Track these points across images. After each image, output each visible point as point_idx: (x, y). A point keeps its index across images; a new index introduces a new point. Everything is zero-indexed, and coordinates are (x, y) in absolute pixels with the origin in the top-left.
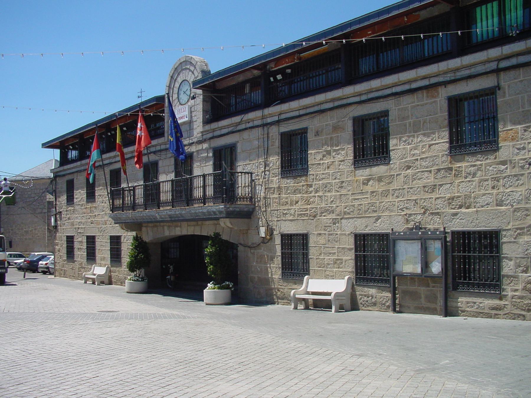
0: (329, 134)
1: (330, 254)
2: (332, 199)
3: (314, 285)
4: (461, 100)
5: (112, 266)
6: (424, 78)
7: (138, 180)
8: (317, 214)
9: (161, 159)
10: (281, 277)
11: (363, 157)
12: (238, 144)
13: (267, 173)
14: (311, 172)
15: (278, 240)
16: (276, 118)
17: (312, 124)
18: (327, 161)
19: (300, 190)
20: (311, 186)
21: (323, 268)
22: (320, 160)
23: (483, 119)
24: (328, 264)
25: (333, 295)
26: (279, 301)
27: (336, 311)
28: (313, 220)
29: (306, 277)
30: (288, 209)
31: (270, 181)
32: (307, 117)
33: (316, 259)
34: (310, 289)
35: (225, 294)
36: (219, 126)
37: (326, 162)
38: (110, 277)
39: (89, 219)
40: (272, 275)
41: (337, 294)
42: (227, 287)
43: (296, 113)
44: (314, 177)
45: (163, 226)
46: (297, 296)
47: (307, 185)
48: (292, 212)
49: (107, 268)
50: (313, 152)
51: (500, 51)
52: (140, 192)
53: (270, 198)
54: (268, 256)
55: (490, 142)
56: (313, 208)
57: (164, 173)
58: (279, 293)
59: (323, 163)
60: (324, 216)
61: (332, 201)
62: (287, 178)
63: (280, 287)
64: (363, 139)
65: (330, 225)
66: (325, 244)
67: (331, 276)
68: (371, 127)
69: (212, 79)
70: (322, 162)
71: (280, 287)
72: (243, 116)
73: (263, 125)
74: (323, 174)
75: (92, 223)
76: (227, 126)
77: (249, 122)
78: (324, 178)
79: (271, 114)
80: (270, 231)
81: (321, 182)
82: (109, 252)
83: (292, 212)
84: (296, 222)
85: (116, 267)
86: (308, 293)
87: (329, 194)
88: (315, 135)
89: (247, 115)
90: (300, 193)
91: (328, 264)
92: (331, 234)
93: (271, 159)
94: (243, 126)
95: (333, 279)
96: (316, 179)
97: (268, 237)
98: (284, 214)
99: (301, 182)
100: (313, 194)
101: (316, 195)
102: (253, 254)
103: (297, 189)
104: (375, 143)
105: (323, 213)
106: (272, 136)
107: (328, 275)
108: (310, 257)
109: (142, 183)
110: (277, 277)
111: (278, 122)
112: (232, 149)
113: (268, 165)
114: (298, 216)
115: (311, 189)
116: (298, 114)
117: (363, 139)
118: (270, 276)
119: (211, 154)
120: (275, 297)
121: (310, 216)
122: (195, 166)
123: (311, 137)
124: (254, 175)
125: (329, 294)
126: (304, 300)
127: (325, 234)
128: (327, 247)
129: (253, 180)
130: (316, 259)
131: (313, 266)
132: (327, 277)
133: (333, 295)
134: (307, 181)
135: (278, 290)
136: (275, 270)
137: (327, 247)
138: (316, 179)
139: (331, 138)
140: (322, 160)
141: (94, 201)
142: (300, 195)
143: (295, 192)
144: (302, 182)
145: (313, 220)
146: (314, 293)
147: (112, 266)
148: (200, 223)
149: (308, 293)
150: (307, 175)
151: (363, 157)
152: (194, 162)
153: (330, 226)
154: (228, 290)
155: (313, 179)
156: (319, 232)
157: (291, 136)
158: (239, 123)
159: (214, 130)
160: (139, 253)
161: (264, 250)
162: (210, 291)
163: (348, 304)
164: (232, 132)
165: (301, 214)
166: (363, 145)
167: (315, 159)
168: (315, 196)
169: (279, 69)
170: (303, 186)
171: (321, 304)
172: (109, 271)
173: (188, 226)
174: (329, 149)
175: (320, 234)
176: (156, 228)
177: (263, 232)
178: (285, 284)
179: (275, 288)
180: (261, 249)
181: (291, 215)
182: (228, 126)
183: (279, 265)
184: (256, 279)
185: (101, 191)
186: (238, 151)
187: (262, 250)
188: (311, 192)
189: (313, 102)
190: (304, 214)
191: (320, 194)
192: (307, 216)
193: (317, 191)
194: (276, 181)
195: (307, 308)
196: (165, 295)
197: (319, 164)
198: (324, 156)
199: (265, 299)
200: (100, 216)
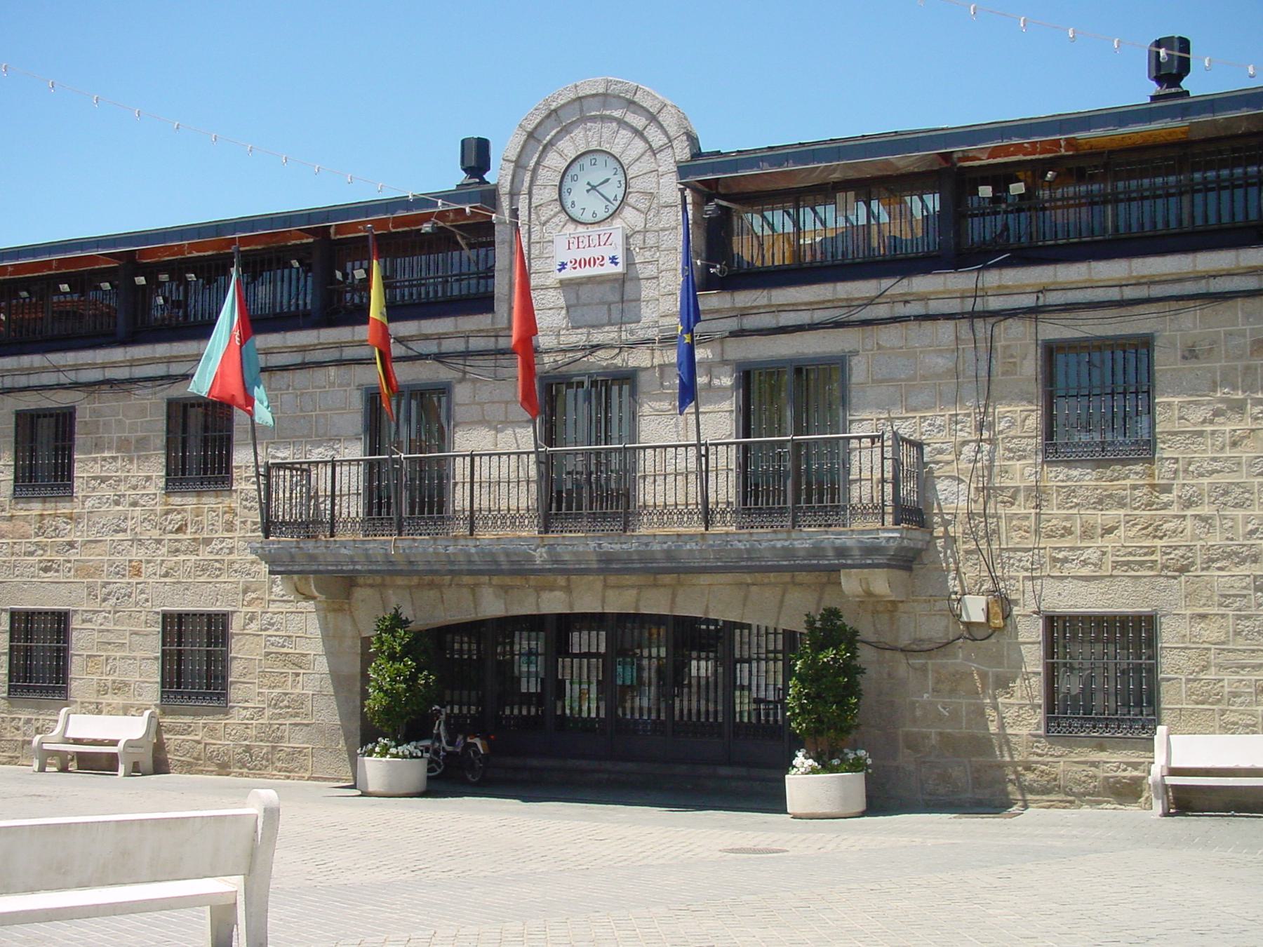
0: (1240, 357)
1: (1243, 668)
2: (1250, 527)
3: (81, 726)
4: (39, 416)
5: (164, 713)
6: (1198, 278)
7: (334, 439)
8: (1193, 564)
9: (462, 380)
10: (1041, 732)
11: (184, 474)
12: (855, 360)
13: (986, 447)
14: (1165, 450)
15: (1030, 634)
16: (1028, 301)
17: (1172, 331)
18: (1228, 426)
19: (1123, 498)
20: (1167, 489)
21: (1212, 704)
22: (1204, 422)
23: (1112, 394)
24: (1236, 695)
25: (121, 744)
26: (1029, 797)
27: (127, 775)
28: (1175, 577)
29: (65, 710)
30: (1072, 549)
31: (996, 470)
32: (1153, 308)
33: (1188, 680)
34: (71, 734)
35: (415, 771)
36: (774, 302)
37: (1228, 429)
38: (159, 747)
39: (32, 554)
40: (1002, 726)
41: (130, 744)
42: (856, 766)
43: (1114, 294)
44: (1180, 465)
45: (474, 588)
46: (46, 747)
47: (1153, 486)
48: (1093, 555)
49: (151, 717)
50: (1176, 400)
51: (1241, 259)
52: (352, 479)
53: (995, 516)
54: (984, 676)
55: (65, 486)
56: (1176, 548)
57: (483, 422)
58: (1030, 776)
59: (1213, 433)
60: (1220, 569)
61: (1253, 532)
62: (29, 499)
63: (1036, 758)
64: (32, 450)
65: (1245, 592)
66: (1223, 643)
67: (1247, 726)
68: (45, 430)
69: (780, 165)
70: (1209, 428)
71: (1036, 758)
72: (892, 281)
73: (973, 315)
74: (1214, 459)
75: (46, 570)
76: (811, 303)
77: (906, 302)
78: (1218, 472)
79: (1007, 287)
80: (1003, 604)
81: (1205, 481)
82: (156, 668)
83: (1093, 555)
84: (1107, 582)
85: (195, 714)
86: (67, 741)
87: (1239, 513)
88: (1184, 357)
89: (905, 281)
90: (1123, 506)
91: (1236, 695)
92: (1248, 617)
93: (1001, 409)
94: (882, 311)
95: (1254, 733)
96: (1186, 471)
97: (998, 622)
98: (1055, 560)
99: (1127, 477)
100: (1175, 510)
101: (1189, 513)
102: (924, 669)
103: (1110, 496)
104: (56, 460)
105: (1214, 561)
106: (1006, 347)
107: (1234, 723)
108: (1161, 676)
109: (356, 451)
110: (1025, 731)
111: (1033, 312)
112: (64, 421)
113: (991, 426)
114: (1114, 568)
115: (1165, 498)
116: (1118, 298)
117: (32, 450)
118: (993, 728)
119: (727, 381)
120: (1010, 788)
121: (1165, 567)
122: (646, 409)
123: (1165, 362)
124: (927, 449)
125: (114, 743)
126: (57, 753)
127: (1223, 616)
128: (1229, 651)
129: (926, 464)
130: (1188, 680)
131: (1169, 698)
132: (1229, 728)
133: (121, 744)
134: (1152, 476)
135: (1028, 768)
136: (1017, 715)
137: (1229, 651)
138: (1186, 471)
139: (1247, 368)
140: (1211, 422)
141: (71, 497)
142: (1122, 512)
143: (1100, 502)
144: (1132, 477)
145: (1175, 577)
146: (77, 741)
147: (164, 713)
148: (667, 579)
149: (67, 741)
150: (1151, 461)
151: (184, 474)
152: (642, 398)
153: (1245, 596)
154: (862, 774)
155: (1176, 472)
156: (1201, 611)
157: (185, 406)
158: (871, 302)
159: (744, 313)
160: (419, 670)
161: (968, 658)
162: (804, 783)
163: (147, 762)
164: (838, 324)
165: (1127, 563)
166: (184, 453)
167: (1181, 418)
168: (1184, 517)
169: (302, 244)
170: (1134, 487)
171: (97, 762)
172: (157, 729)
173: (606, 586)
174: (1240, 395)
175: (1203, 617)
176: (433, 594)
177: (975, 609)
178: (1059, 750)
179: (1014, 764)
180: (956, 657)
181: (1085, 563)
182: (812, 306)
183: (1033, 698)
184: (934, 740)
185: (113, 466)
186: (854, 380)
187: (962, 658)
188: (1166, 506)
189: (829, 296)
190: (1141, 563)
191: (1205, 510)
192: (1151, 568)
193: (1189, 504)
194: (1022, 472)
195: (64, 769)
196: (525, 800)
197: (1200, 434)
198: (1217, 413)
199: (969, 795)
200: (99, 548)
